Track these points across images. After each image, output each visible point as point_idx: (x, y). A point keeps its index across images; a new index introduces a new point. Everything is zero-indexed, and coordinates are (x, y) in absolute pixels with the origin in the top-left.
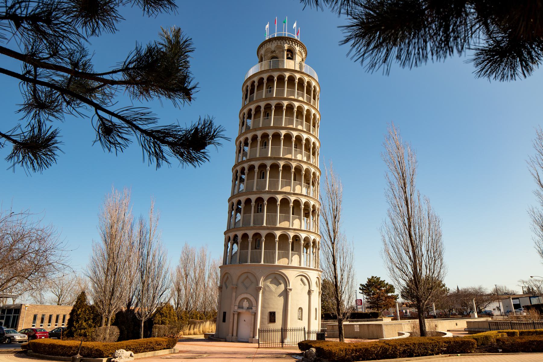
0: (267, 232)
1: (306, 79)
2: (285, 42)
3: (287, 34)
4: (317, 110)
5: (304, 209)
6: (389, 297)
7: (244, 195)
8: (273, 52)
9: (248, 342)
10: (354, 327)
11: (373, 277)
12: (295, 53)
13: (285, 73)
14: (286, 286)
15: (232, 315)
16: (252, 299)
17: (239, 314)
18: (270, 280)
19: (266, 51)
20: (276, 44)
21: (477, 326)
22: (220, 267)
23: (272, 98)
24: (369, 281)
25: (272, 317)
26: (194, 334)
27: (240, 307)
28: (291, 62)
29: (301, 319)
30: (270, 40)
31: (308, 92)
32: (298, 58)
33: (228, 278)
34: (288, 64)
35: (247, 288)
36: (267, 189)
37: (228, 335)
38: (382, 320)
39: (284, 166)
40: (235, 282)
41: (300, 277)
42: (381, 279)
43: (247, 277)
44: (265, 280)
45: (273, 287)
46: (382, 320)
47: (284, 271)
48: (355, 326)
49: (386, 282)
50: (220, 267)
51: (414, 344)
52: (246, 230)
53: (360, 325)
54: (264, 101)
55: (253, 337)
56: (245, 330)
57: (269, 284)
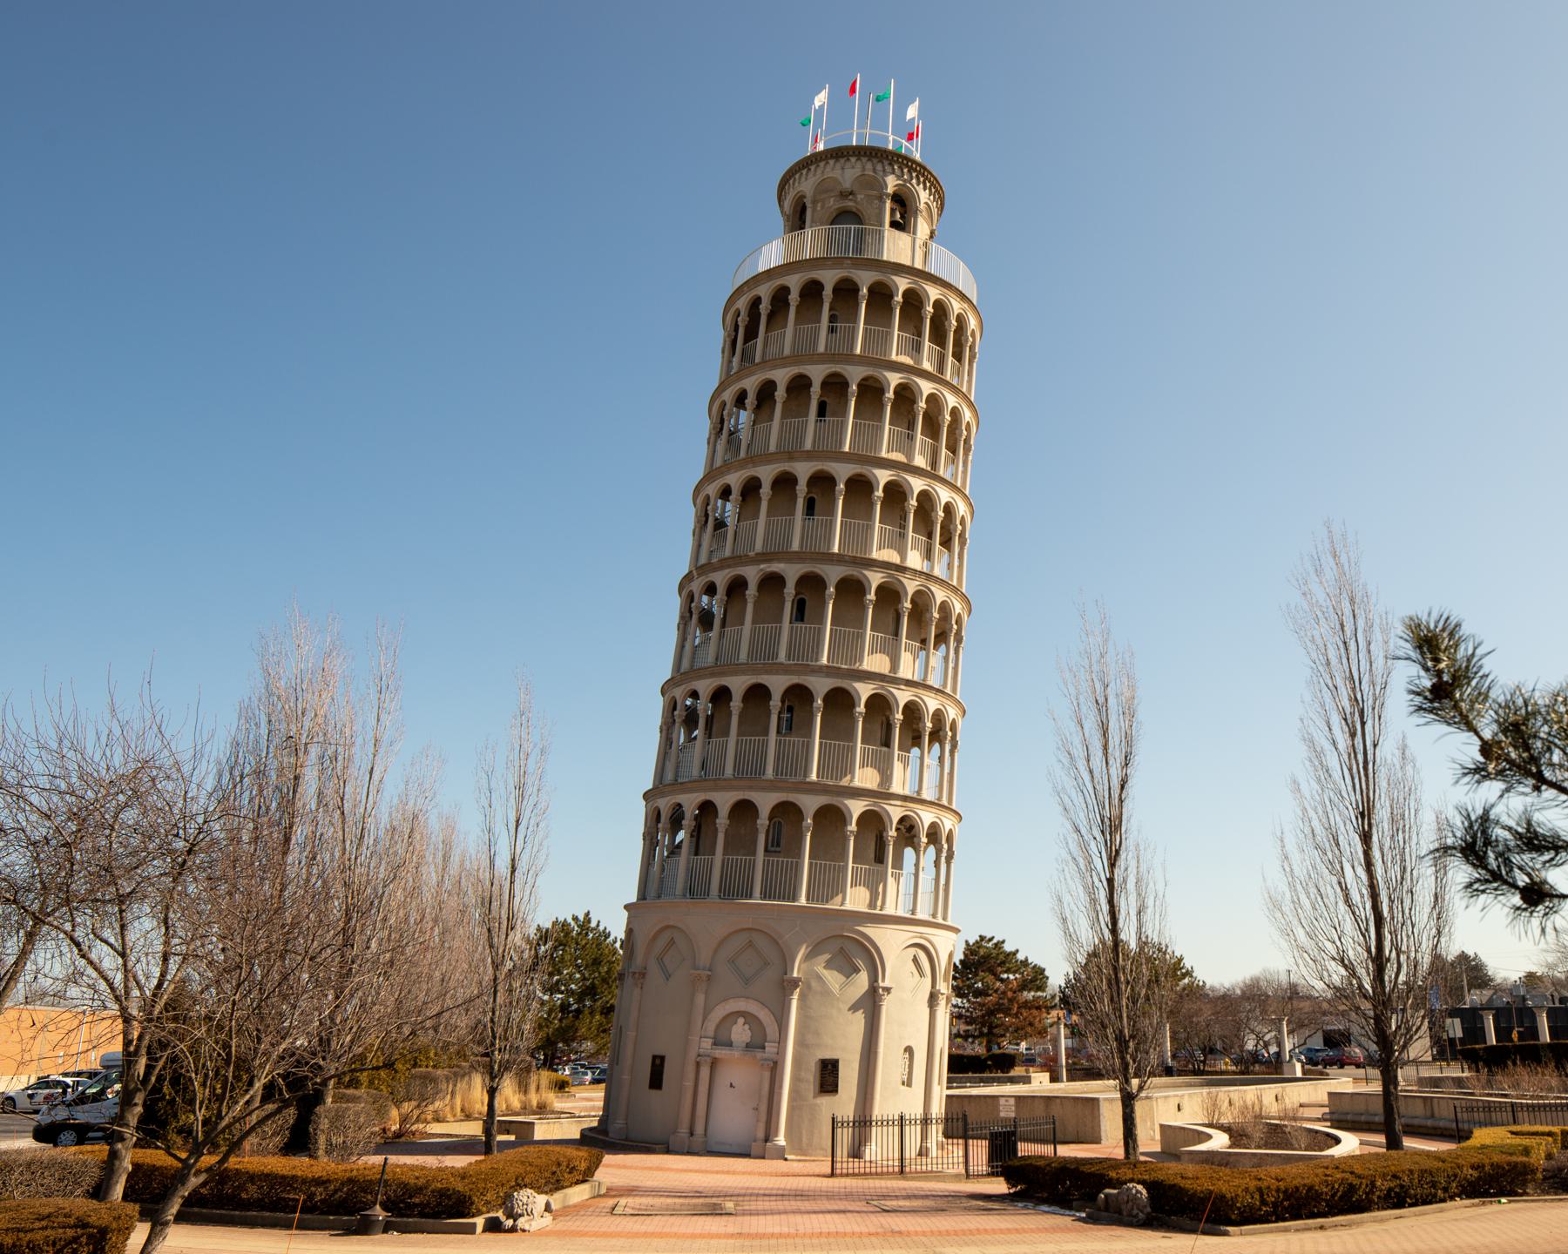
0: (822, 800)
1: (956, 306)
2: (888, 168)
3: (891, 141)
4: (966, 398)
5: (904, 724)
6: (1026, 1005)
7: (744, 673)
8: (844, 195)
9: (747, 1155)
10: (998, 1105)
11: (982, 938)
12: (916, 211)
13: (897, 279)
14: (874, 979)
15: (691, 1068)
16: (764, 1015)
17: (714, 1063)
18: (827, 956)
19: (822, 189)
20: (857, 171)
21: (1361, 1107)
22: (626, 907)
23: (851, 359)
24: (971, 950)
25: (828, 1076)
26: (438, 1120)
27: (722, 1041)
28: (903, 239)
29: (908, 1083)
30: (839, 154)
31: (939, 337)
32: (923, 228)
33: (672, 942)
34: (896, 247)
35: (747, 981)
36: (824, 661)
37: (675, 1132)
38: (1026, 1080)
39: (880, 588)
40: (704, 957)
41: (913, 951)
42: (1008, 948)
43: (751, 944)
44: (809, 957)
45: (833, 979)
46: (1026, 1080)
47: (872, 931)
48: (1002, 1101)
49: (1020, 957)
50: (626, 907)
51: (1411, 1171)
52: (751, 788)
53: (1019, 1099)
54: (823, 362)
55: (766, 1140)
56: (731, 1115)
57: (820, 970)
